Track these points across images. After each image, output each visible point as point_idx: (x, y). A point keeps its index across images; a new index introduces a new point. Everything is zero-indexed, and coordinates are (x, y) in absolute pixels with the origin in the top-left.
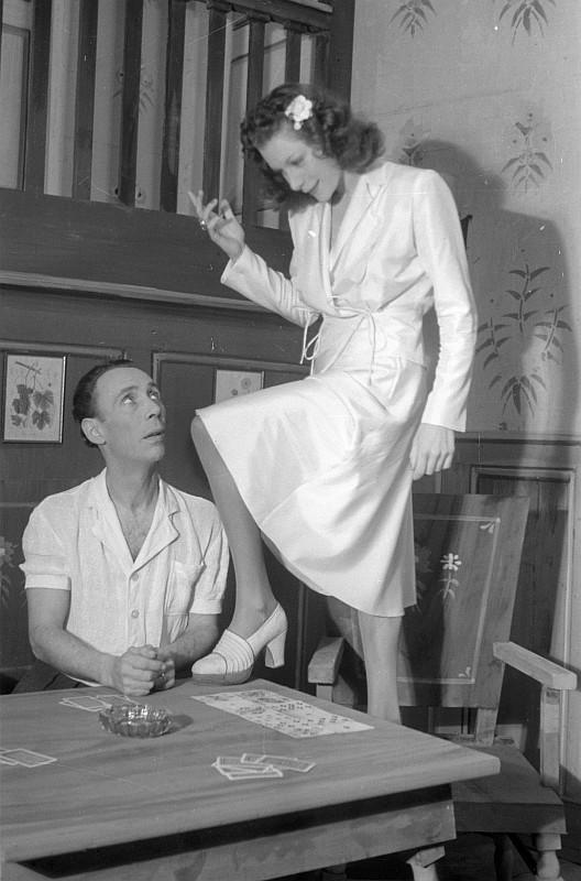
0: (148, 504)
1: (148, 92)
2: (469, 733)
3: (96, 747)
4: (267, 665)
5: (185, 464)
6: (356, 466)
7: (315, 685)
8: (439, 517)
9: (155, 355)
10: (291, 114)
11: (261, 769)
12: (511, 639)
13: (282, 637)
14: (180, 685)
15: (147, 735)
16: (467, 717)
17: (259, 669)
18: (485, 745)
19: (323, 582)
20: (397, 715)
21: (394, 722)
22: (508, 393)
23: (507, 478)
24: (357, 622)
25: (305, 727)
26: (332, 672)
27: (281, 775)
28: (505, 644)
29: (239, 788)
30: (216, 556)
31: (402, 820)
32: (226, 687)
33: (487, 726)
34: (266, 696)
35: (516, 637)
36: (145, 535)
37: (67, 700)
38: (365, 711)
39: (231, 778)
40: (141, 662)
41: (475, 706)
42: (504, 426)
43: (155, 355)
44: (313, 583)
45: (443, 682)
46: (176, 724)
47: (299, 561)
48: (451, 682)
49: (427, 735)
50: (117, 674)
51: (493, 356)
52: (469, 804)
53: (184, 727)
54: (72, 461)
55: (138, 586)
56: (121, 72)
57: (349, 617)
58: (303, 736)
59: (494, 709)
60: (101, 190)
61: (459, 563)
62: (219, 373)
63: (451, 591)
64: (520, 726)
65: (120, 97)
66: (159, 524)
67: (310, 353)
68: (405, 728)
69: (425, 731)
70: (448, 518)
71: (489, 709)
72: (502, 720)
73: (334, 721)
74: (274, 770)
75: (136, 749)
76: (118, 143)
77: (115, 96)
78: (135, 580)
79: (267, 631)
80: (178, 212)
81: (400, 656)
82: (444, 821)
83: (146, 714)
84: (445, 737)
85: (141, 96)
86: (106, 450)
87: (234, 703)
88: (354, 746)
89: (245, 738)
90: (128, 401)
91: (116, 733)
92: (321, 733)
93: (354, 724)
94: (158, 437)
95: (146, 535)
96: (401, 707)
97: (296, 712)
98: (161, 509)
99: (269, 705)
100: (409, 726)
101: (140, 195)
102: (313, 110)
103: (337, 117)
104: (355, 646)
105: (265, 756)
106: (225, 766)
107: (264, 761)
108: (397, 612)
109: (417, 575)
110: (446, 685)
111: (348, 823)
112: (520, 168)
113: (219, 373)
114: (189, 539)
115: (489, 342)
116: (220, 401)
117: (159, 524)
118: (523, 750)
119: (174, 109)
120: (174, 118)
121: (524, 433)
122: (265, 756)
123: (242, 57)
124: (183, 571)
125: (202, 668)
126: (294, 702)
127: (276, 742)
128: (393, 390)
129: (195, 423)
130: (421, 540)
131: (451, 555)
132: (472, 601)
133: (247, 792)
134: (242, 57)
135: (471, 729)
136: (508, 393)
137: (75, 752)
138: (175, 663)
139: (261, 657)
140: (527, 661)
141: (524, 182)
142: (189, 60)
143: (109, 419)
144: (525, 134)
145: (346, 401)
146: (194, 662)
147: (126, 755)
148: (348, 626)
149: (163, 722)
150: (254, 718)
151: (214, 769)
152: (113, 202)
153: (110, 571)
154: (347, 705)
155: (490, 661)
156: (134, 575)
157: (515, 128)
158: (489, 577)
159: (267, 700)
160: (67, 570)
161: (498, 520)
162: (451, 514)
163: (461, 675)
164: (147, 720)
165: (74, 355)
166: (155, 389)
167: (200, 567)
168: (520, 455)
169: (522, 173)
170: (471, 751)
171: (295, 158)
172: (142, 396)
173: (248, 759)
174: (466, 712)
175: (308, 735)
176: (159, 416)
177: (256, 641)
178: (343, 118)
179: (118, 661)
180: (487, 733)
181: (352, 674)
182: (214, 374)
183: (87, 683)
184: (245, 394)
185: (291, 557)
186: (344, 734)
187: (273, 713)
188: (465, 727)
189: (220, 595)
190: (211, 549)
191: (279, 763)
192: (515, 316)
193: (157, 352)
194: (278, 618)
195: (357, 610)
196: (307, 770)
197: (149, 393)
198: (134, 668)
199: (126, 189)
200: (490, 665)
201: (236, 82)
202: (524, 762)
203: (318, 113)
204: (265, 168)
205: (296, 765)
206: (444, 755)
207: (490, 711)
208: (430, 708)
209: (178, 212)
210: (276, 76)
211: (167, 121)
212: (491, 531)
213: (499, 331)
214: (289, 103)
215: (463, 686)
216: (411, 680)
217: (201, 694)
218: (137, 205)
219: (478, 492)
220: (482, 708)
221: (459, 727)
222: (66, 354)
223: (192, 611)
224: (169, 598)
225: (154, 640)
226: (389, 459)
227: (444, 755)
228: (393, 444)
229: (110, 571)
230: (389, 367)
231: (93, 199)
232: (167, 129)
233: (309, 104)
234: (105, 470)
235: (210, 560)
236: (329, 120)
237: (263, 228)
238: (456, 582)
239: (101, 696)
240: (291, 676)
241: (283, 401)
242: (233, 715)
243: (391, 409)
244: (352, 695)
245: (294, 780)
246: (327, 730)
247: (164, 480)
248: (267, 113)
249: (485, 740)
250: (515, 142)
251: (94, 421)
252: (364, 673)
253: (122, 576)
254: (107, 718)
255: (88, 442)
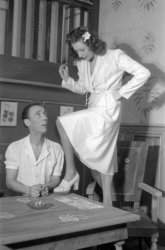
0: (41, 145)
1: (41, 27)
2: (131, 208)
3: (26, 212)
4: (74, 189)
5: (54, 133)
6: (103, 134)
7: (88, 195)
8: (123, 148)
9: (43, 102)
10: (84, 37)
11: (73, 219)
12: (143, 182)
13: (78, 182)
14: (50, 195)
15: (41, 209)
16: (131, 204)
17: (72, 191)
18: (136, 212)
19: (92, 166)
20: (111, 203)
21: (111, 206)
22: (143, 113)
23: (144, 137)
24: (100, 177)
25: (85, 207)
26: (93, 192)
27: (78, 220)
28: (141, 183)
29: (67, 224)
30: (60, 159)
31: (112, 233)
32: (63, 196)
33: (137, 207)
34: (74, 198)
35: (145, 181)
36: (40, 154)
37: (19, 199)
38: (102, 202)
39: (64, 221)
40: (37, 188)
41: (133, 201)
42: (142, 122)
43: (43, 102)
44: (90, 166)
45: (124, 194)
46: (49, 206)
47: (86, 160)
48: (127, 194)
49: (120, 209)
50: (30, 191)
51: (139, 102)
52: (131, 228)
53: (51, 207)
54: (20, 131)
55: (38, 168)
56: (33, 22)
57: (98, 176)
58: (84, 209)
59: (139, 202)
60: (28, 55)
61: (129, 161)
62: (61, 107)
63: (127, 169)
64: (146, 207)
65: (33, 28)
66: (44, 150)
67: (88, 102)
68: (114, 207)
69: (119, 208)
70: (126, 148)
71: (137, 202)
72: (140, 205)
73: (93, 205)
74: (77, 219)
75: (38, 213)
76: (33, 41)
77: (31, 29)
78: (37, 166)
79: (73, 180)
80: (50, 61)
81: (112, 187)
82: (125, 234)
83: (40, 203)
84: (125, 210)
85: (39, 28)
86: (30, 129)
87: (65, 200)
88: (98, 212)
89: (68, 210)
90: (38, 115)
91: (32, 208)
92: (90, 209)
93: (99, 206)
94: (46, 126)
95: (40, 154)
96: (112, 201)
97: (83, 203)
98: (45, 146)
99: (75, 200)
100: (115, 207)
101: (39, 56)
102: (90, 37)
103: (96, 40)
104: (99, 184)
105: (74, 215)
106: (62, 218)
107: (74, 216)
108: (112, 174)
109: (118, 164)
110: (126, 195)
111: (97, 234)
112: (146, 49)
113: (61, 107)
114: (53, 154)
115: (137, 98)
116: (61, 116)
117: (44, 150)
118: (147, 213)
119: (48, 33)
120: (48, 35)
121: (148, 124)
122: (74, 215)
123: (67, 18)
124: (51, 164)
125: (56, 190)
126: (82, 200)
127: (76, 211)
128: (113, 112)
129: (57, 121)
130: (119, 154)
131: (126, 158)
132: (133, 171)
133: (67, 225)
134: (67, 18)
135: (132, 207)
136: (143, 113)
137: (20, 214)
138: (48, 189)
139: (72, 187)
140: (148, 188)
141: (147, 53)
142: (53, 18)
143: (32, 120)
144: (147, 39)
145: (100, 115)
146: (54, 189)
147: (35, 215)
148: (97, 178)
149: (45, 205)
150: (71, 204)
151: (60, 219)
152: (31, 58)
153: (30, 163)
154: (97, 201)
155: (138, 188)
156: (37, 165)
157: (145, 38)
158: (137, 165)
159: (75, 199)
160: (17, 164)
161: (140, 149)
162: (127, 147)
163: (129, 192)
164: (41, 205)
165: (20, 102)
166: (46, 113)
167: (56, 163)
168: (147, 130)
169: (147, 51)
170: (132, 214)
171: (82, 49)
172: (42, 114)
173: (69, 216)
174: (131, 203)
175: (86, 209)
176: (46, 120)
177: (71, 183)
178: (97, 41)
179: (31, 187)
180: (136, 209)
181: (99, 191)
182: (60, 107)
183: (24, 195)
184: (69, 113)
185: (84, 158)
186: (96, 209)
187: (76, 203)
188: (130, 207)
189: (61, 170)
190: (59, 157)
191: (77, 217)
192: (145, 91)
193: (43, 101)
194: (77, 176)
195: (100, 173)
196: (86, 219)
197: (44, 113)
198: (35, 189)
199: (35, 55)
200: (138, 189)
201: (66, 25)
202: (147, 217)
203: (91, 38)
204: (71, 48)
205: (82, 217)
206: (124, 215)
207: (137, 203)
208: (121, 202)
209: (50, 61)
210: (77, 24)
211: (47, 35)
212: (138, 152)
213: (141, 99)
214: (84, 34)
215: (130, 195)
216: (115, 194)
217: (56, 198)
218: (38, 59)
219: (134, 141)
220: (135, 202)
221: (129, 207)
222: (18, 101)
223: (53, 175)
224: (47, 171)
225: (43, 183)
226: (111, 132)
227: (124, 215)
228: (113, 127)
229: (30, 163)
230: (112, 106)
231: (25, 57)
232: (46, 37)
233: (89, 35)
234: (29, 135)
235: (59, 161)
236: (94, 41)
237: (73, 66)
238: (128, 166)
239: (28, 198)
240: (81, 192)
241: (81, 115)
242: (64, 203)
243: (113, 117)
244: (98, 198)
245: (82, 222)
246: (91, 208)
247: (46, 138)
248: (76, 34)
249: (136, 211)
250: (145, 42)
251: (28, 120)
252: (102, 191)
253: (34, 165)
254: (29, 204)
255: (25, 125)
